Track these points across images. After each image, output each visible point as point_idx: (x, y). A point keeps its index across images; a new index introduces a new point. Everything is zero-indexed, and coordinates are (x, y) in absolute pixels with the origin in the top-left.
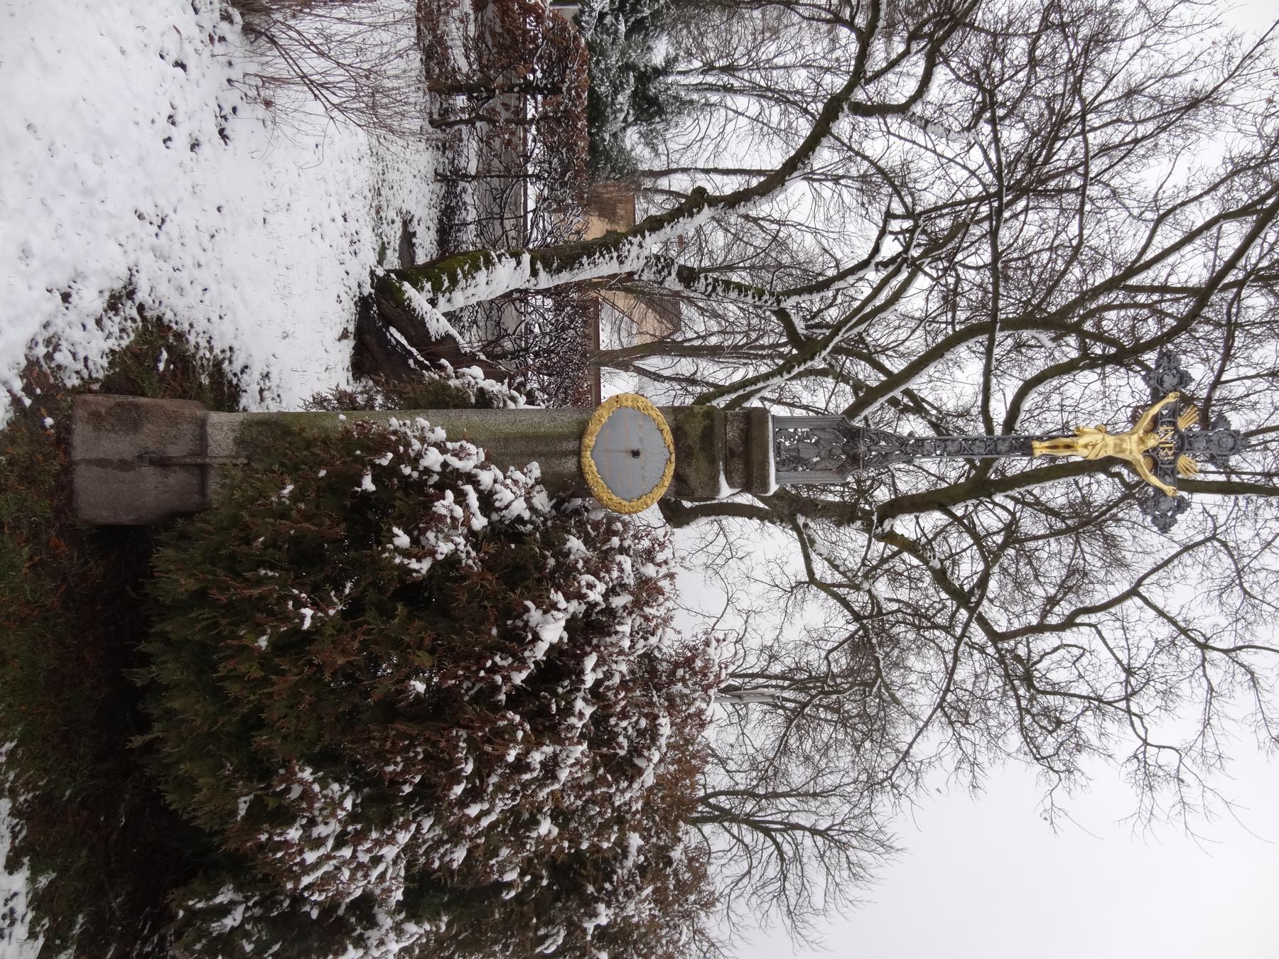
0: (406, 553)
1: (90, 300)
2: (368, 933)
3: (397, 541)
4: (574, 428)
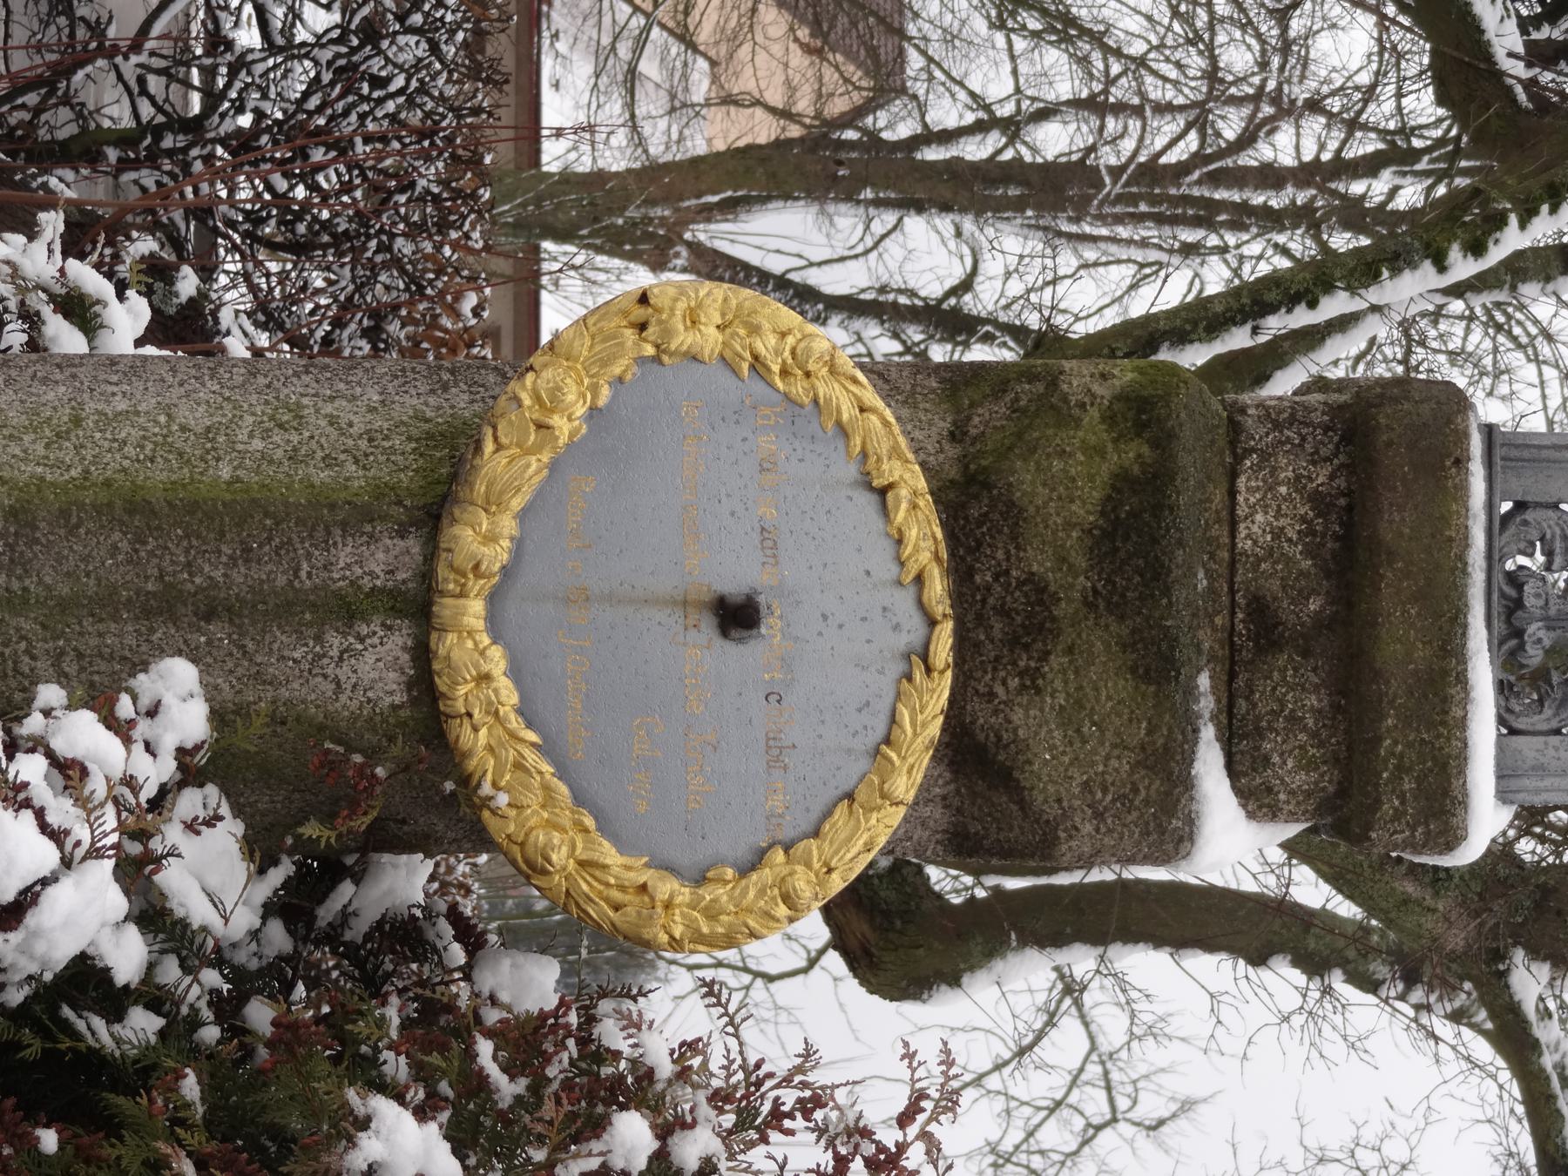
4: (400, 467)
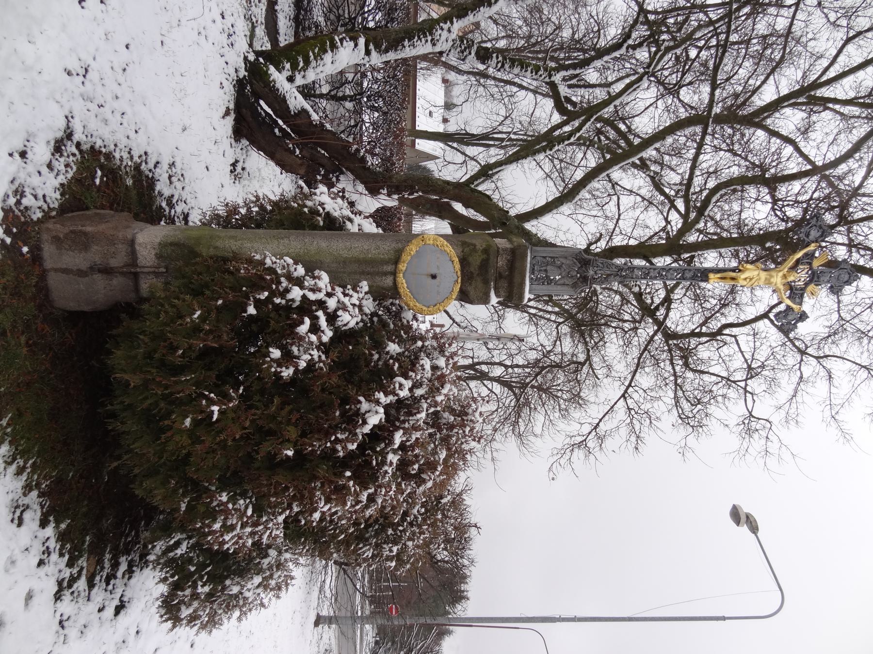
1: (41, 153)
2: (263, 561)
3: (272, 356)
4: (392, 256)
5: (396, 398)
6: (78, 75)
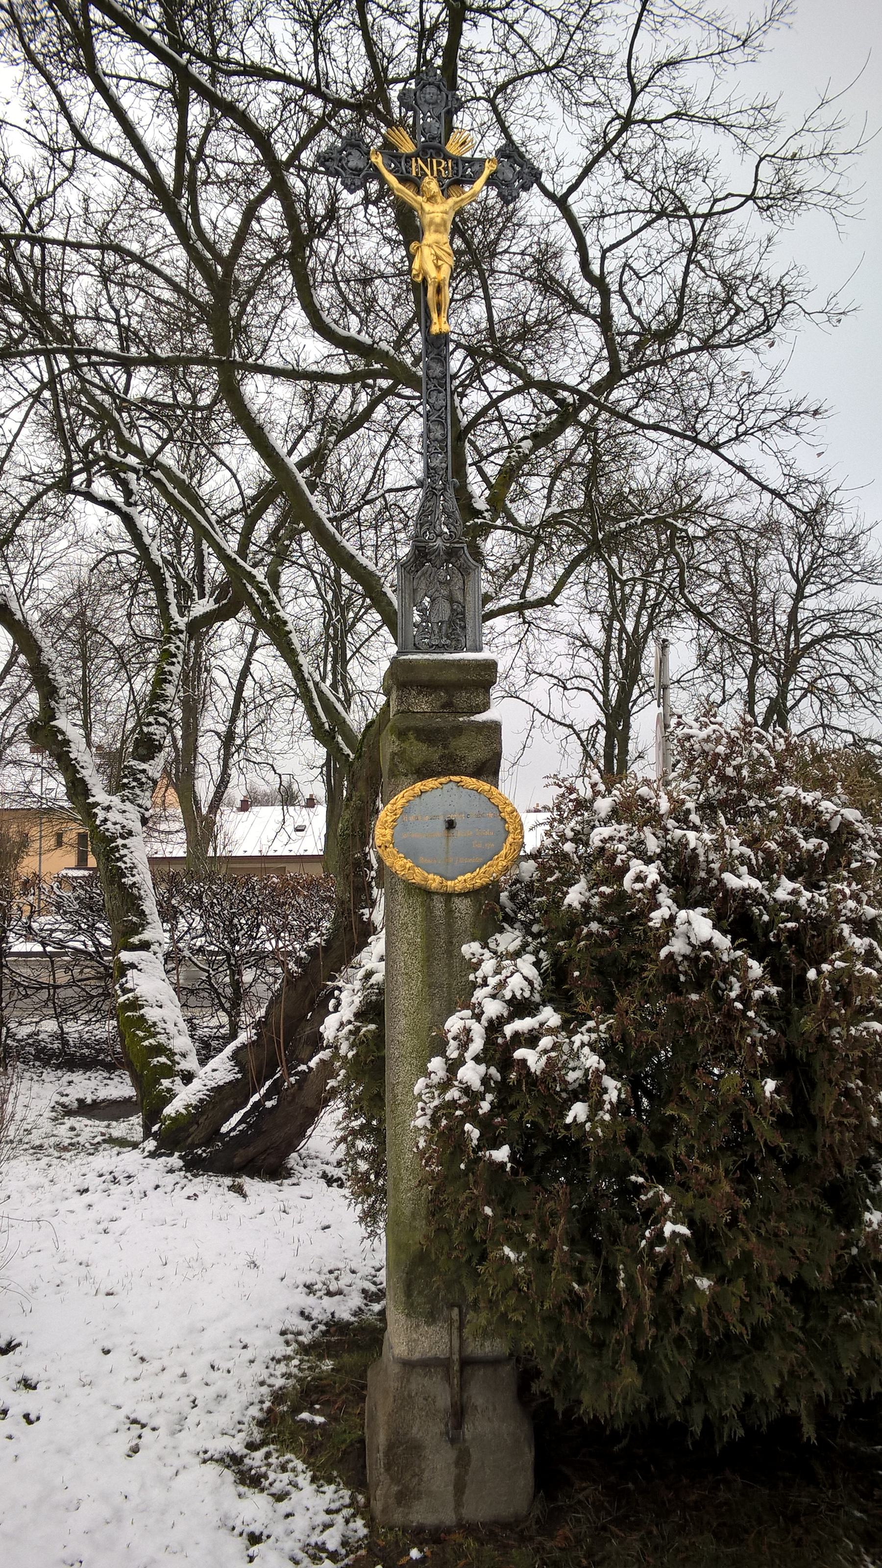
0: (596, 1107)
1: (255, 1509)
3: (582, 1118)
5: (663, 887)
6: (140, 1437)
